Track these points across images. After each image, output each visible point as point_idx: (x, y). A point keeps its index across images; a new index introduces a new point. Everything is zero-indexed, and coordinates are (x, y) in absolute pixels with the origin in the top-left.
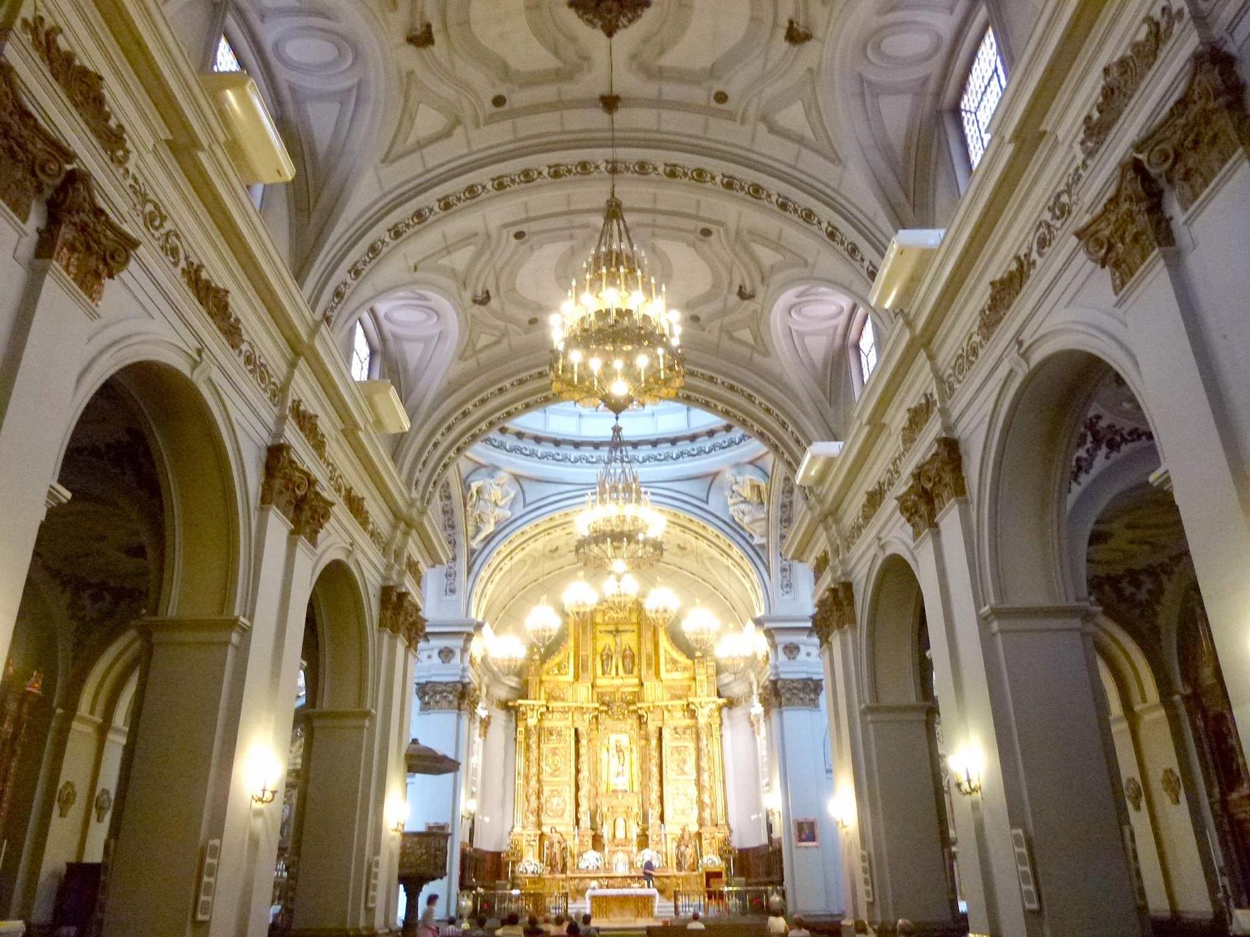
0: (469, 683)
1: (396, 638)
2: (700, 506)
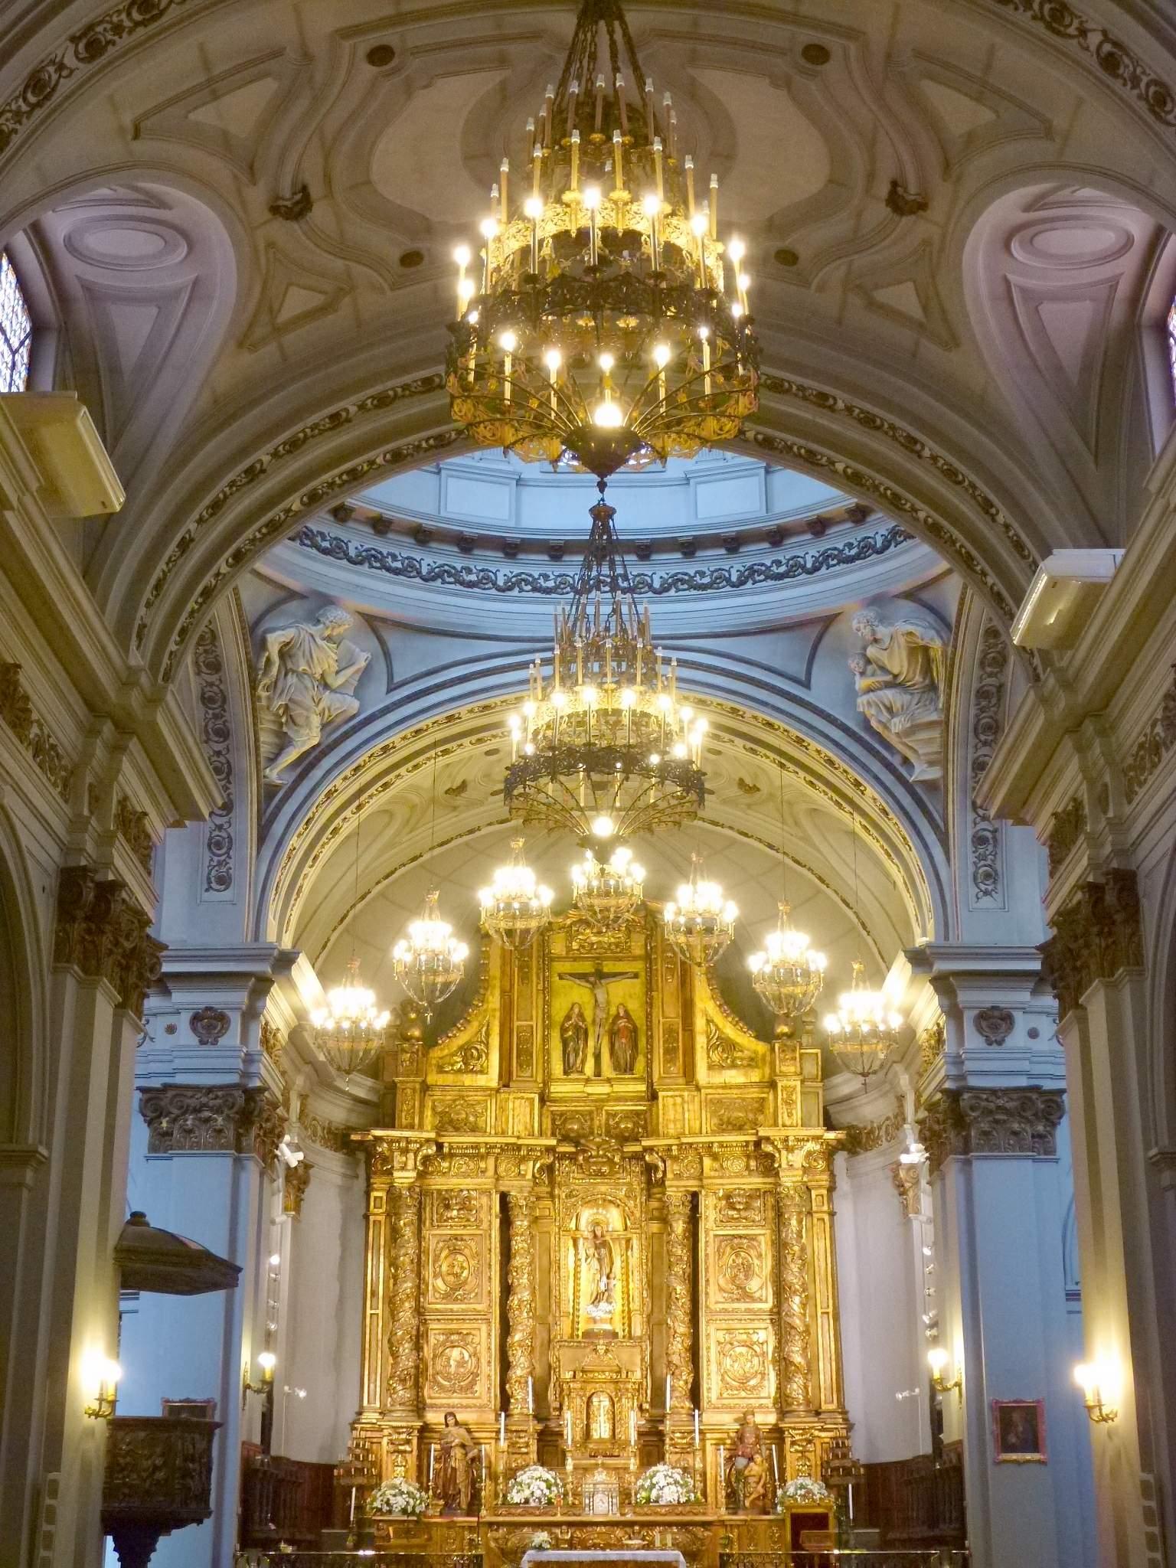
0: (261, 1090)
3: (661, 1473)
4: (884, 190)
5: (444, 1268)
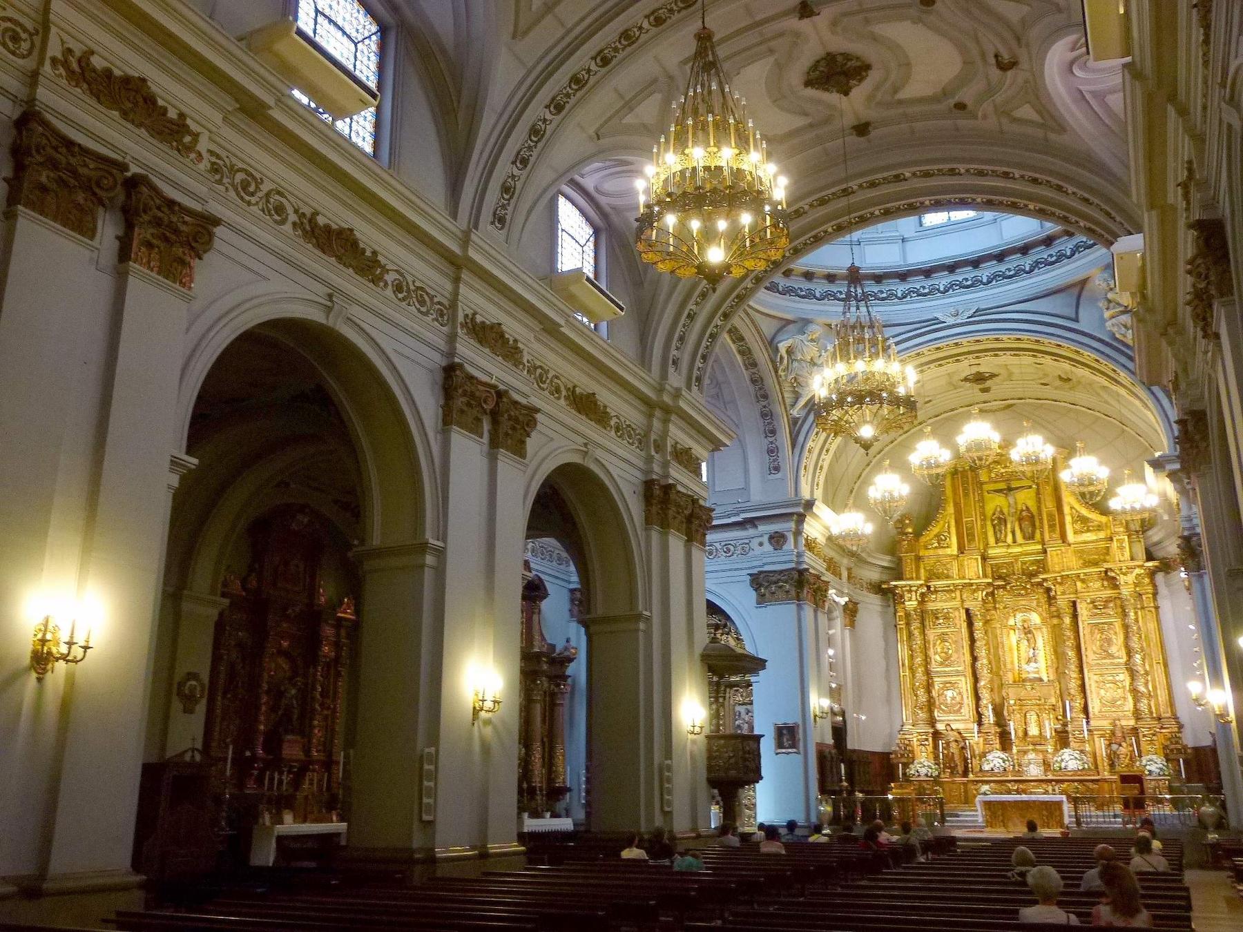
0: (807, 570)
1: (667, 534)
2: (1069, 328)
3: (1066, 753)
4: (993, 61)
5: (939, 650)
